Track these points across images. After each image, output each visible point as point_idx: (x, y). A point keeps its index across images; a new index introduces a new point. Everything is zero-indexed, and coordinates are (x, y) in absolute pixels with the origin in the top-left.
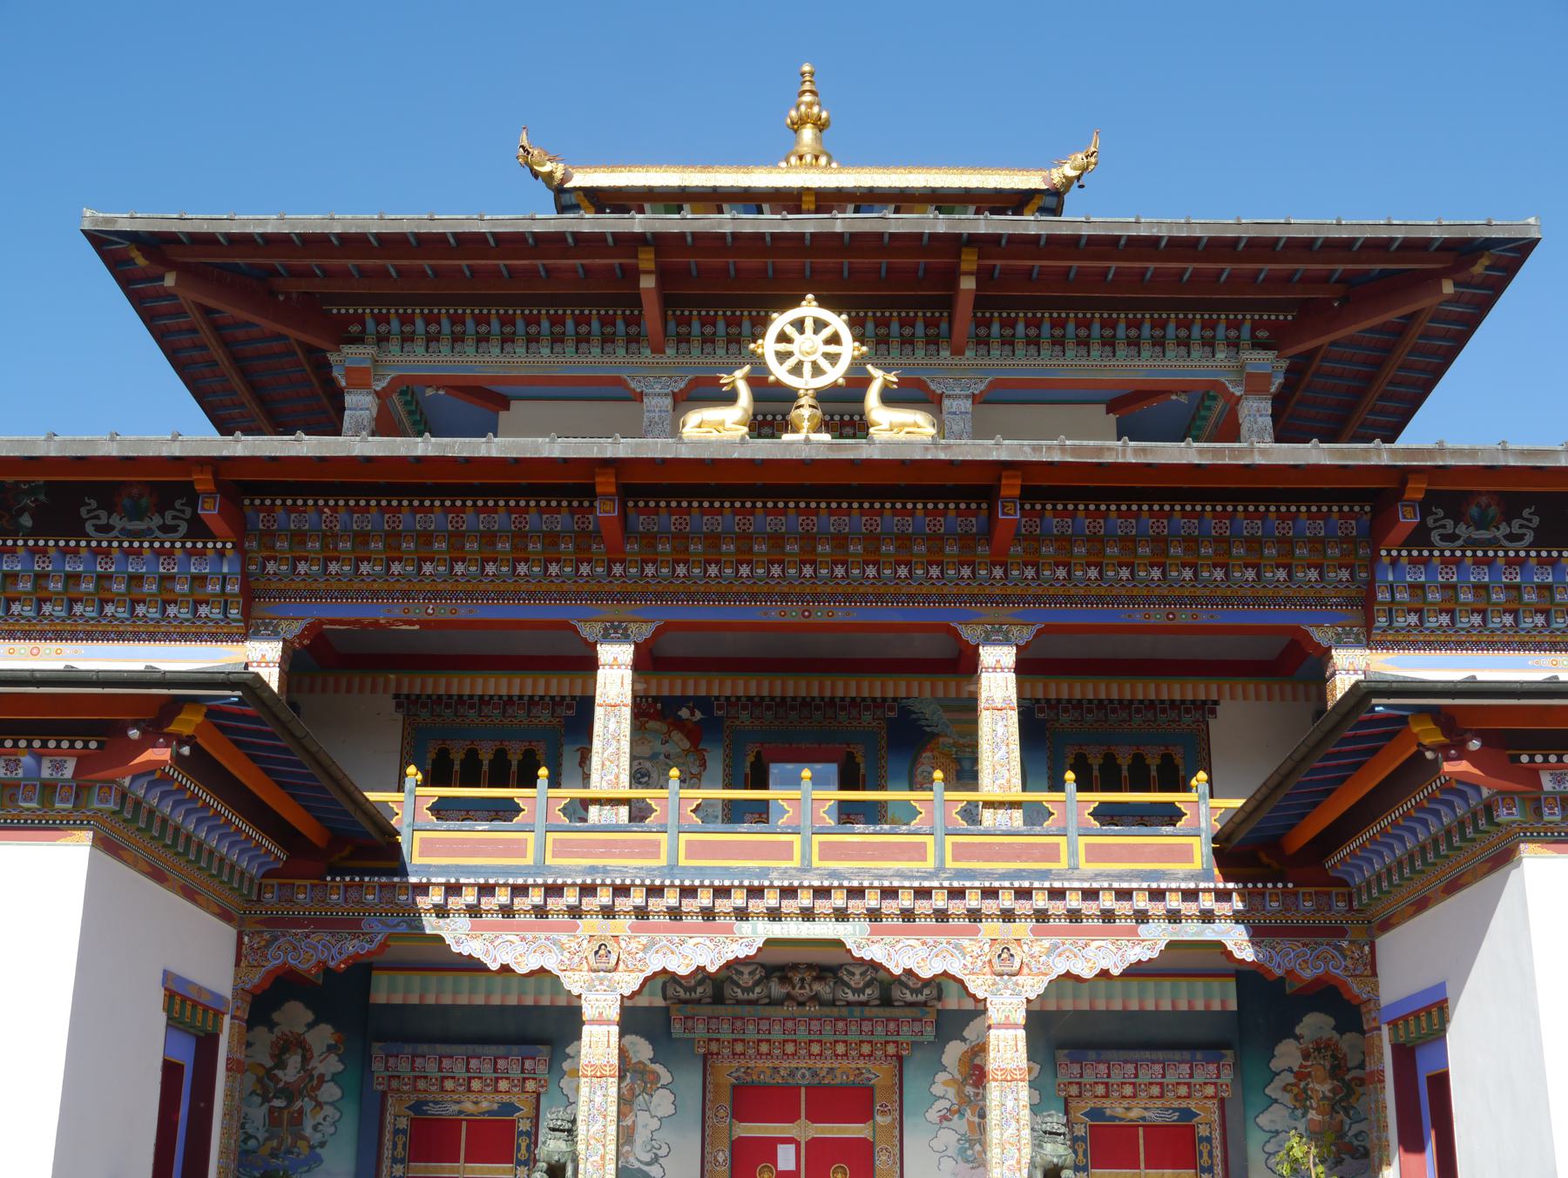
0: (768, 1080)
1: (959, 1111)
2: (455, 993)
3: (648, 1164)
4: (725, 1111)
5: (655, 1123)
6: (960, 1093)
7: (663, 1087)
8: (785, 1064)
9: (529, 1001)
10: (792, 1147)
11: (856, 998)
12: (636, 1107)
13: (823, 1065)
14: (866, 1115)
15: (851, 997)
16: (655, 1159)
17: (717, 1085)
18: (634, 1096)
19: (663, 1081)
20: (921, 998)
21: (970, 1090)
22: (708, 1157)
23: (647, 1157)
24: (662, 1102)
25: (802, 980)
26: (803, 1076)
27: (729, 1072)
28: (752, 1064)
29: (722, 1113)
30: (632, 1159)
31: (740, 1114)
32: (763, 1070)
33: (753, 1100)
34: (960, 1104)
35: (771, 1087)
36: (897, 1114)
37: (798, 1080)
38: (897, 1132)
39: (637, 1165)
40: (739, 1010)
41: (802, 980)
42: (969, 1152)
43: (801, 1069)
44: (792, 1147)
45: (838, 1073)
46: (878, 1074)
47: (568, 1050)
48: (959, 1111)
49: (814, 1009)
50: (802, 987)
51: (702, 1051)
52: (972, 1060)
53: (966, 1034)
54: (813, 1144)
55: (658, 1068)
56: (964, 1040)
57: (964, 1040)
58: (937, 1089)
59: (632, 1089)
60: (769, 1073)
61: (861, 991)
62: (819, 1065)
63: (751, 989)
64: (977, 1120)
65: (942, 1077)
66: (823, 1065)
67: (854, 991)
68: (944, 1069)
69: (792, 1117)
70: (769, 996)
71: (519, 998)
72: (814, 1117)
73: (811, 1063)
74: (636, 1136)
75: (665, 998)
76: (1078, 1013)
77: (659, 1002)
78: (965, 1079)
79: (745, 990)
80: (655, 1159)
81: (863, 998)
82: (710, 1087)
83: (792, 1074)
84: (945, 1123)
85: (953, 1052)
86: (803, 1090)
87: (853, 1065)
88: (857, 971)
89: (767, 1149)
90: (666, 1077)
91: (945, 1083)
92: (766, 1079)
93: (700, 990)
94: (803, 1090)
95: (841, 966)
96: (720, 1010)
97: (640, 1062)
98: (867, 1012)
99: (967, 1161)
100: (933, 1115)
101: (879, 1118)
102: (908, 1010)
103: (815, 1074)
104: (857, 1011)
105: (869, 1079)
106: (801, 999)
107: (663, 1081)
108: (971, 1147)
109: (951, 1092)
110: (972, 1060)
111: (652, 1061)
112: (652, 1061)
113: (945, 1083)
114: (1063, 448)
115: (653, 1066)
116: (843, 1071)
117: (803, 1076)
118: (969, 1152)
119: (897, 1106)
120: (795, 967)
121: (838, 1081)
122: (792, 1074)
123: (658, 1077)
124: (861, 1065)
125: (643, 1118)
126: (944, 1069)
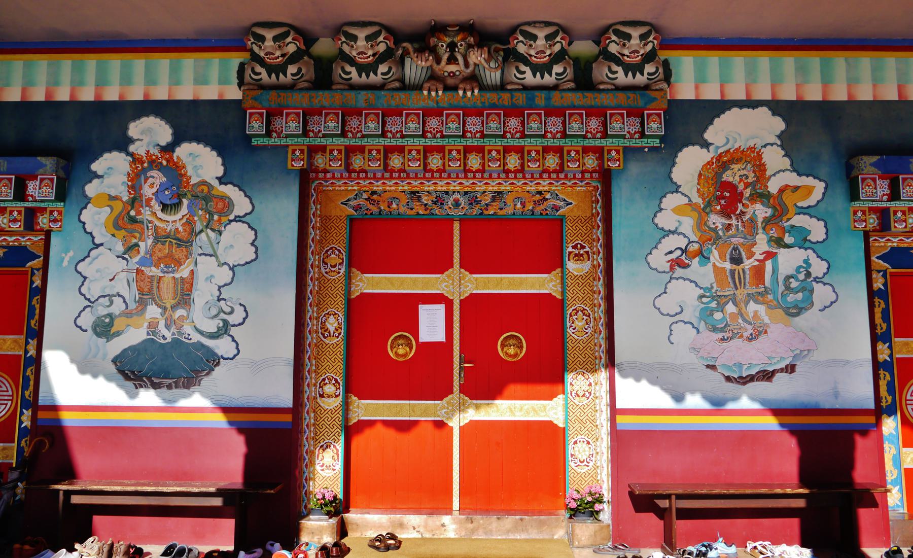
0: (402, 210)
1: (700, 253)
2: (151, 80)
3: (213, 336)
4: (338, 259)
5: (225, 275)
6: (701, 224)
7: (238, 219)
8: (429, 186)
9: (38, 95)
10: (440, 309)
11: (537, 80)
12: (195, 250)
13: (485, 187)
14: (550, 260)
15: (530, 78)
16: (225, 329)
17: (326, 220)
18: (194, 233)
19: (238, 211)
20: (640, 79)
21: (716, 220)
22: (311, 325)
23: (211, 326)
24: (236, 241)
25: (452, 46)
26: (457, 204)
27: (345, 196)
28: (378, 186)
29: (334, 259)
30: (188, 329)
31: (361, 259)
32: (395, 194)
33: (380, 240)
34: (702, 243)
35: (409, 221)
36: (600, 259)
37: (448, 209)
38: (600, 286)
39: (196, 338)
40: (360, 99)
41: (452, 46)
42: (718, 316)
43: (454, 192)
44: (440, 309)
45: (509, 199)
46: (570, 199)
47: (95, 167)
48: (700, 253)
49: (470, 95)
50: (452, 60)
51: (298, 165)
52: (718, 175)
53: (708, 135)
54: (472, 303)
55: (230, 191)
56: (706, 145)
57: (706, 145)
58: (666, 220)
59: (190, 223)
60: (404, 199)
61: (545, 68)
62: (480, 187)
63: (370, 68)
64: (728, 266)
65: (672, 201)
66: (485, 187)
67: (536, 69)
68: (677, 189)
69: (441, 265)
70: (402, 80)
71: (24, 91)
72: (472, 265)
73: (467, 183)
74: (195, 294)
75: (241, 84)
76: (879, 105)
77: (234, 93)
78: (709, 204)
79: (362, 69)
80: (225, 329)
81: (549, 80)
82: (315, 221)
83: (439, 201)
84: (679, 272)
85: (690, 163)
86: (457, 226)
87: (532, 187)
88: (541, 34)
89: (405, 310)
90: (241, 204)
91: (677, 210)
92: (401, 208)
93: (292, 69)
94: (457, 226)
95: (513, 30)
96: (322, 98)
97: (204, 183)
98: (557, 99)
99: (715, 329)
100: (659, 259)
101: (572, 266)
102: (621, 97)
103: (474, 201)
104: (540, 99)
105: (556, 208)
106: (450, 81)
107: (238, 211)
108: (721, 308)
109: (688, 224)
110: (718, 175)
111: (221, 180)
112: (221, 180)
113: (677, 210)
114: (488, 532)
115: (223, 188)
116: (516, 196)
117: (457, 204)
118: (718, 316)
119: (599, 246)
120: (439, 29)
121: (509, 210)
122: (439, 201)
123: (229, 205)
124: (544, 185)
125: (206, 266)
126: (677, 189)
